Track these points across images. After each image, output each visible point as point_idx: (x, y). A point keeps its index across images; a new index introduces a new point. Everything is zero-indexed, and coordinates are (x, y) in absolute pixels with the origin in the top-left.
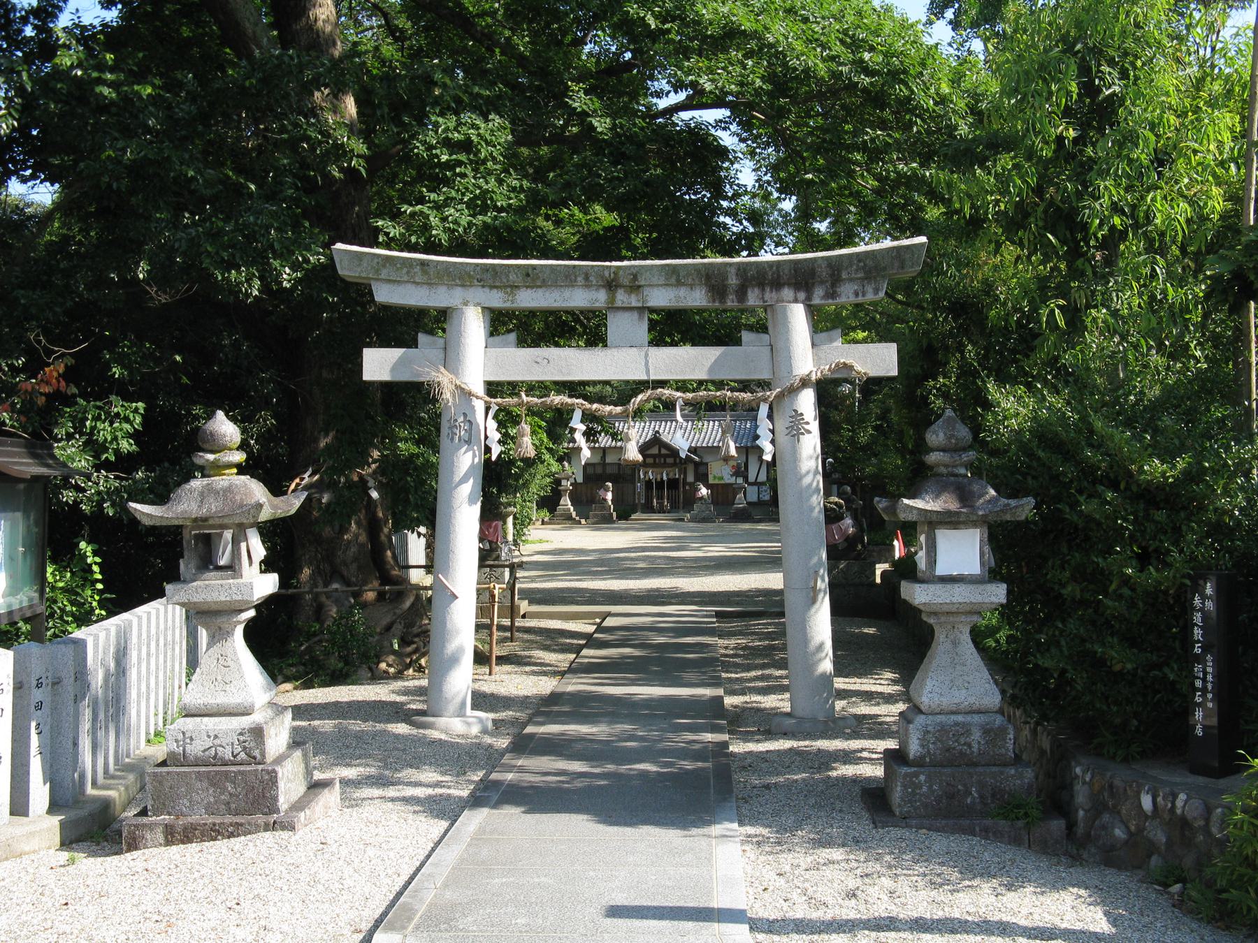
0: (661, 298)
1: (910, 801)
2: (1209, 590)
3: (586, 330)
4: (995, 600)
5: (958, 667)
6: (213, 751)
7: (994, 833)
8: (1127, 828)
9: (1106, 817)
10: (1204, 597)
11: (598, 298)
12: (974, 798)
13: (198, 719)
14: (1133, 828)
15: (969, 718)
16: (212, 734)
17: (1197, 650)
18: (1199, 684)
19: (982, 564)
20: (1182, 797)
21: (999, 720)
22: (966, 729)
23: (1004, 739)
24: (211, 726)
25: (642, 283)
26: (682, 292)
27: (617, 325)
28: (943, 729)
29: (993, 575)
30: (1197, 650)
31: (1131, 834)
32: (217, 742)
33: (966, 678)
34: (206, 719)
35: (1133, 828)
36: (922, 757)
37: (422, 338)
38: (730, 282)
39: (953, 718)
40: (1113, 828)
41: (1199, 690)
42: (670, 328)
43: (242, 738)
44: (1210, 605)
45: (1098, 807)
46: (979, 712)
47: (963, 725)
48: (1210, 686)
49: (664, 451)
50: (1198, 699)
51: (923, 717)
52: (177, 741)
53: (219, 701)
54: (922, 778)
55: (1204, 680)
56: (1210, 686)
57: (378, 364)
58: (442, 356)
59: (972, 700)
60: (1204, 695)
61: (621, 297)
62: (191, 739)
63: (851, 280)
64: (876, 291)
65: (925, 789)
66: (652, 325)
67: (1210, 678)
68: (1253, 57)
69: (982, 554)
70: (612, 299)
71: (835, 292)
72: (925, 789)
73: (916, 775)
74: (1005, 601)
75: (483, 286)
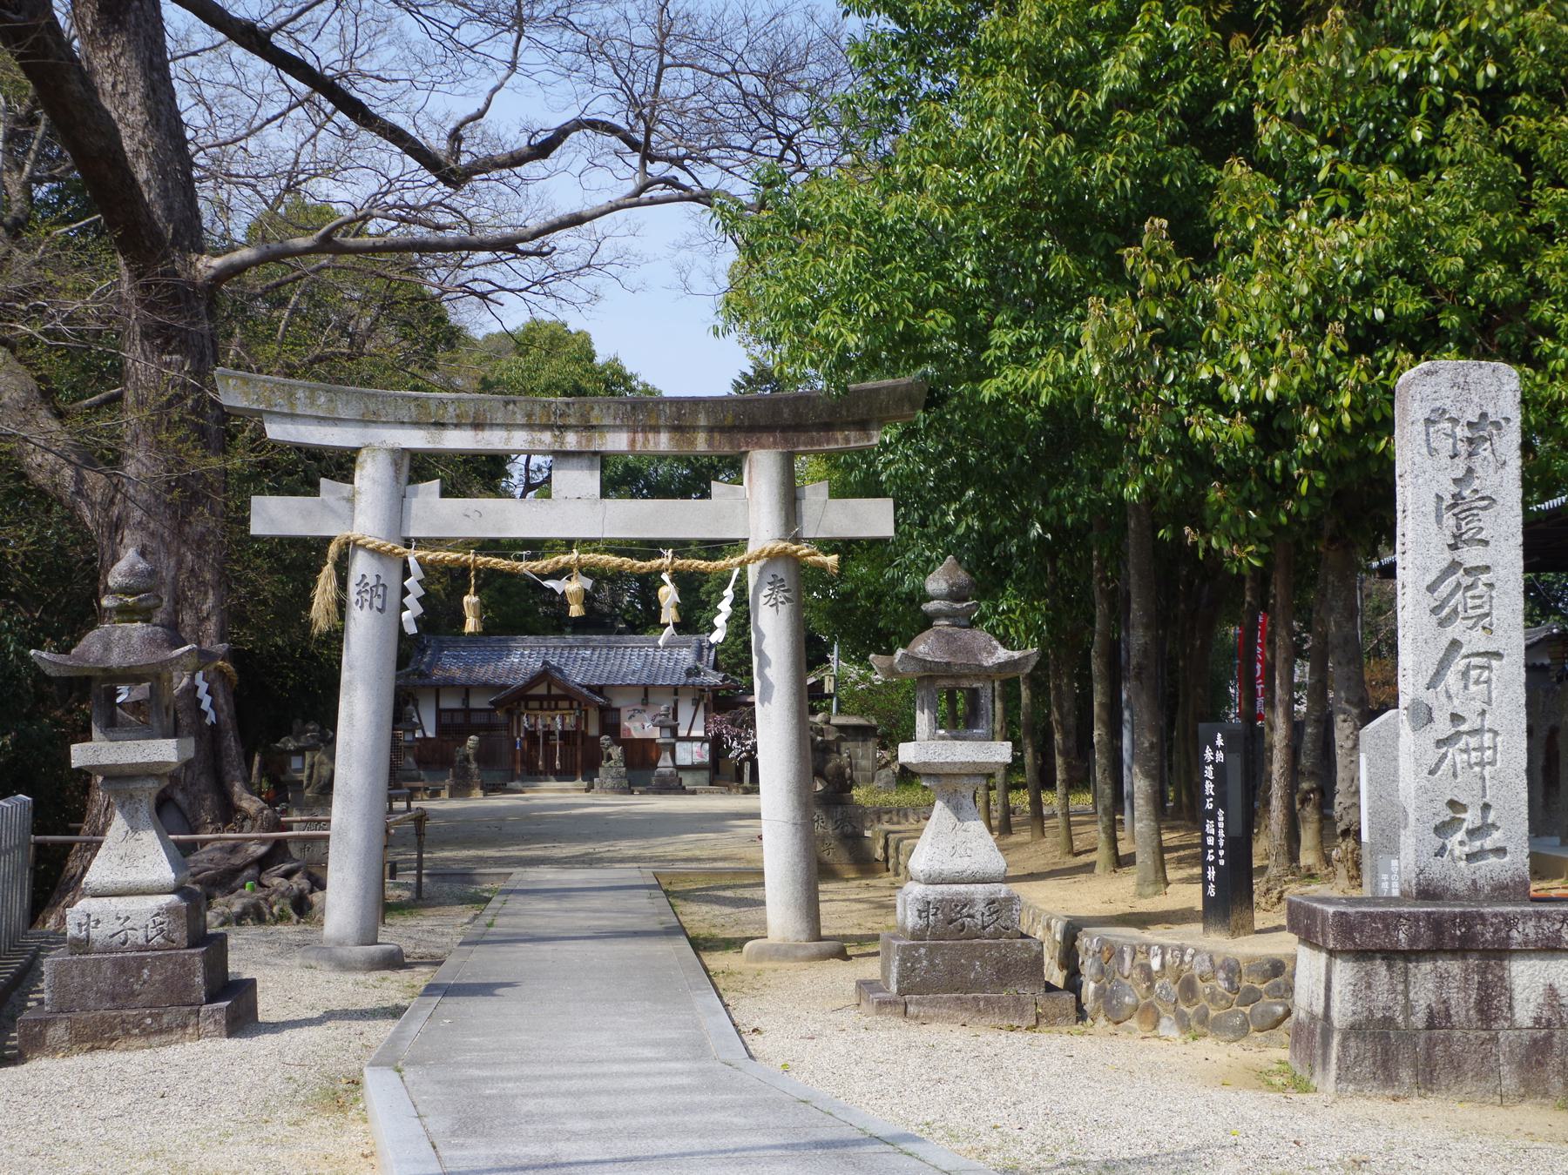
2: (1220, 742)
4: (998, 759)
6: (122, 935)
10: (1215, 749)
13: (106, 900)
15: (972, 887)
16: (123, 916)
17: (1209, 806)
18: (1210, 841)
24: (121, 907)
28: (943, 904)
30: (1209, 806)
32: (128, 924)
34: (114, 900)
38: (475, 599)
39: (955, 888)
43: (158, 920)
48: (1221, 843)
49: (555, 691)
52: (80, 925)
53: (129, 878)
55: (1216, 837)
56: (1221, 843)
57: (274, 516)
59: (975, 868)
60: (1216, 854)
65: (925, 963)
67: (1221, 833)
68: (197, 215)
72: (925, 963)
73: (916, 948)
74: (1010, 760)
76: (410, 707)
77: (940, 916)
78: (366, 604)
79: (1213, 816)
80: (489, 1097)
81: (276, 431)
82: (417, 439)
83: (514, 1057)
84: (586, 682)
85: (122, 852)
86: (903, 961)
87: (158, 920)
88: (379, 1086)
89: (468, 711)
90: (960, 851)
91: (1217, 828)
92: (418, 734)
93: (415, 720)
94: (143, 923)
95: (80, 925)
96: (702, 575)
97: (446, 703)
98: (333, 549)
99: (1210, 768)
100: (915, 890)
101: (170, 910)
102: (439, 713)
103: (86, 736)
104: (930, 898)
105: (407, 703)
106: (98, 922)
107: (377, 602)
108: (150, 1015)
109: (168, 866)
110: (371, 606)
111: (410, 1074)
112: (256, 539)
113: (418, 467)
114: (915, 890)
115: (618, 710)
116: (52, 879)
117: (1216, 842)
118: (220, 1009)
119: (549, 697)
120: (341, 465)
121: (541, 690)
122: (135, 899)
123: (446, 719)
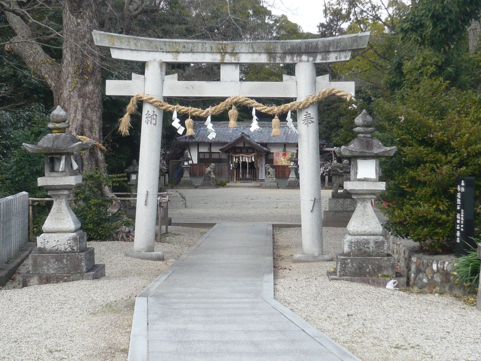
0: (246, 59)
1: (344, 270)
2: (463, 184)
3: (211, 73)
5: (365, 217)
7: (377, 283)
8: (428, 278)
9: (421, 275)
10: (461, 186)
11: (216, 58)
12: (370, 269)
13: (51, 234)
14: (430, 278)
15: (369, 237)
19: (376, 174)
20: (447, 263)
21: (381, 238)
22: (367, 242)
23: (383, 246)
25: (238, 51)
26: (256, 56)
27: (224, 71)
28: (358, 243)
29: (381, 179)
30: (458, 208)
31: (429, 280)
32: (58, 243)
33: (369, 221)
34: (53, 234)
35: (430, 278)
36: (350, 253)
37: (134, 75)
39: (363, 237)
40: (423, 279)
41: (458, 224)
42: (251, 73)
43: (69, 242)
44: (463, 189)
45: (418, 271)
46: (373, 235)
47: (367, 240)
48: (462, 222)
50: (458, 228)
51: (350, 236)
52: (41, 243)
53: (59, 227)
54: (349, 260)
55: (460, 220)
57: (114, 88)
58: (143, 84)
59: (370, 230)
61: (228, 58)
62: (48, 242)
63: (335, 52)
64: (346, 57)
65: (350, 265)
66: (242, 72)
67: (462, 219)
69: (376, 170)
70: (223, 59)
71: (326, 57)
72: (350, 265)
73: (346, 259)
75: (163, 52)
76: (187, 151)
77: (356, 247)
78: (149, 122)
79: (459, 212)
80: (176, 309)
81: (116, 54)
82: (169, 58)
83: (189, 295)
84: (259, 141)
85: (56, 217)
86: (341, 264)
87: (69, 242)
88: (140, 303)
89: (211, 153)
90: (365, 223)
91: (461, 217)
92: (190, 162)
93: (189, 156)
94: (63, 243)
95: (41, 243)
96: (279, 110)
97: (202, 150)
98: (131, 107)
99: (459, 193)
100: (348, 238)
101: (75, 239)
102: (199, 153)
103: (42, 175)
104: (353, 241)
105: (186, 149)
106: (48, 242)
107: (153, 122)
108: (66, 276)
109: (72, 223)
110: (151, 123)
111: (150, 300)
112: (107, 96)
113: (172, 68)
114: (348, 238)
115: (273, 153)
116: (35, 225)
117: (460, 222)
118: (91, 275)
119: (244, 147)
120: (140, 68)
121: (241, 145)
122: (60, 234)
123: (202, 156)
